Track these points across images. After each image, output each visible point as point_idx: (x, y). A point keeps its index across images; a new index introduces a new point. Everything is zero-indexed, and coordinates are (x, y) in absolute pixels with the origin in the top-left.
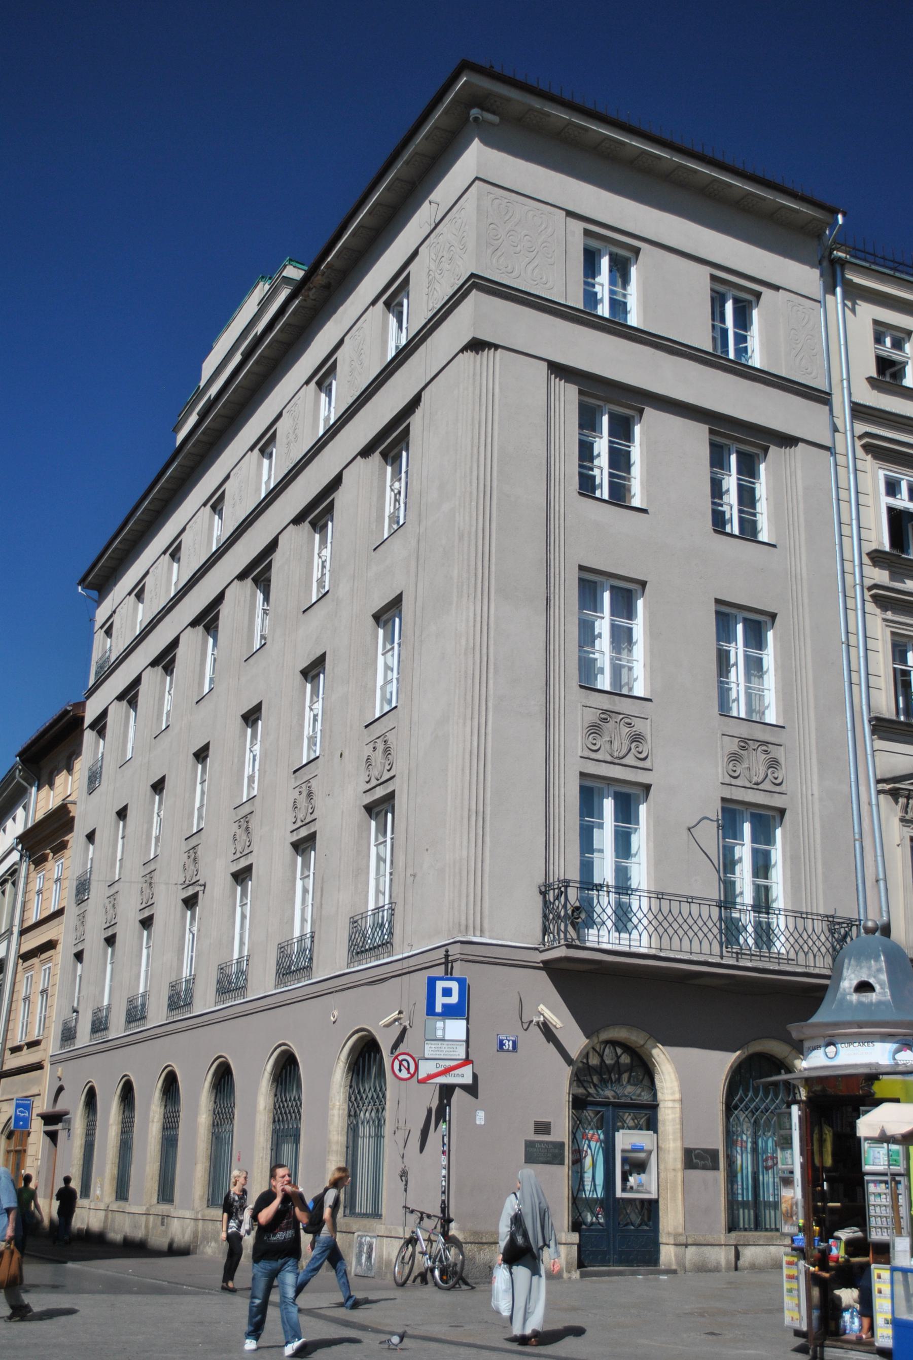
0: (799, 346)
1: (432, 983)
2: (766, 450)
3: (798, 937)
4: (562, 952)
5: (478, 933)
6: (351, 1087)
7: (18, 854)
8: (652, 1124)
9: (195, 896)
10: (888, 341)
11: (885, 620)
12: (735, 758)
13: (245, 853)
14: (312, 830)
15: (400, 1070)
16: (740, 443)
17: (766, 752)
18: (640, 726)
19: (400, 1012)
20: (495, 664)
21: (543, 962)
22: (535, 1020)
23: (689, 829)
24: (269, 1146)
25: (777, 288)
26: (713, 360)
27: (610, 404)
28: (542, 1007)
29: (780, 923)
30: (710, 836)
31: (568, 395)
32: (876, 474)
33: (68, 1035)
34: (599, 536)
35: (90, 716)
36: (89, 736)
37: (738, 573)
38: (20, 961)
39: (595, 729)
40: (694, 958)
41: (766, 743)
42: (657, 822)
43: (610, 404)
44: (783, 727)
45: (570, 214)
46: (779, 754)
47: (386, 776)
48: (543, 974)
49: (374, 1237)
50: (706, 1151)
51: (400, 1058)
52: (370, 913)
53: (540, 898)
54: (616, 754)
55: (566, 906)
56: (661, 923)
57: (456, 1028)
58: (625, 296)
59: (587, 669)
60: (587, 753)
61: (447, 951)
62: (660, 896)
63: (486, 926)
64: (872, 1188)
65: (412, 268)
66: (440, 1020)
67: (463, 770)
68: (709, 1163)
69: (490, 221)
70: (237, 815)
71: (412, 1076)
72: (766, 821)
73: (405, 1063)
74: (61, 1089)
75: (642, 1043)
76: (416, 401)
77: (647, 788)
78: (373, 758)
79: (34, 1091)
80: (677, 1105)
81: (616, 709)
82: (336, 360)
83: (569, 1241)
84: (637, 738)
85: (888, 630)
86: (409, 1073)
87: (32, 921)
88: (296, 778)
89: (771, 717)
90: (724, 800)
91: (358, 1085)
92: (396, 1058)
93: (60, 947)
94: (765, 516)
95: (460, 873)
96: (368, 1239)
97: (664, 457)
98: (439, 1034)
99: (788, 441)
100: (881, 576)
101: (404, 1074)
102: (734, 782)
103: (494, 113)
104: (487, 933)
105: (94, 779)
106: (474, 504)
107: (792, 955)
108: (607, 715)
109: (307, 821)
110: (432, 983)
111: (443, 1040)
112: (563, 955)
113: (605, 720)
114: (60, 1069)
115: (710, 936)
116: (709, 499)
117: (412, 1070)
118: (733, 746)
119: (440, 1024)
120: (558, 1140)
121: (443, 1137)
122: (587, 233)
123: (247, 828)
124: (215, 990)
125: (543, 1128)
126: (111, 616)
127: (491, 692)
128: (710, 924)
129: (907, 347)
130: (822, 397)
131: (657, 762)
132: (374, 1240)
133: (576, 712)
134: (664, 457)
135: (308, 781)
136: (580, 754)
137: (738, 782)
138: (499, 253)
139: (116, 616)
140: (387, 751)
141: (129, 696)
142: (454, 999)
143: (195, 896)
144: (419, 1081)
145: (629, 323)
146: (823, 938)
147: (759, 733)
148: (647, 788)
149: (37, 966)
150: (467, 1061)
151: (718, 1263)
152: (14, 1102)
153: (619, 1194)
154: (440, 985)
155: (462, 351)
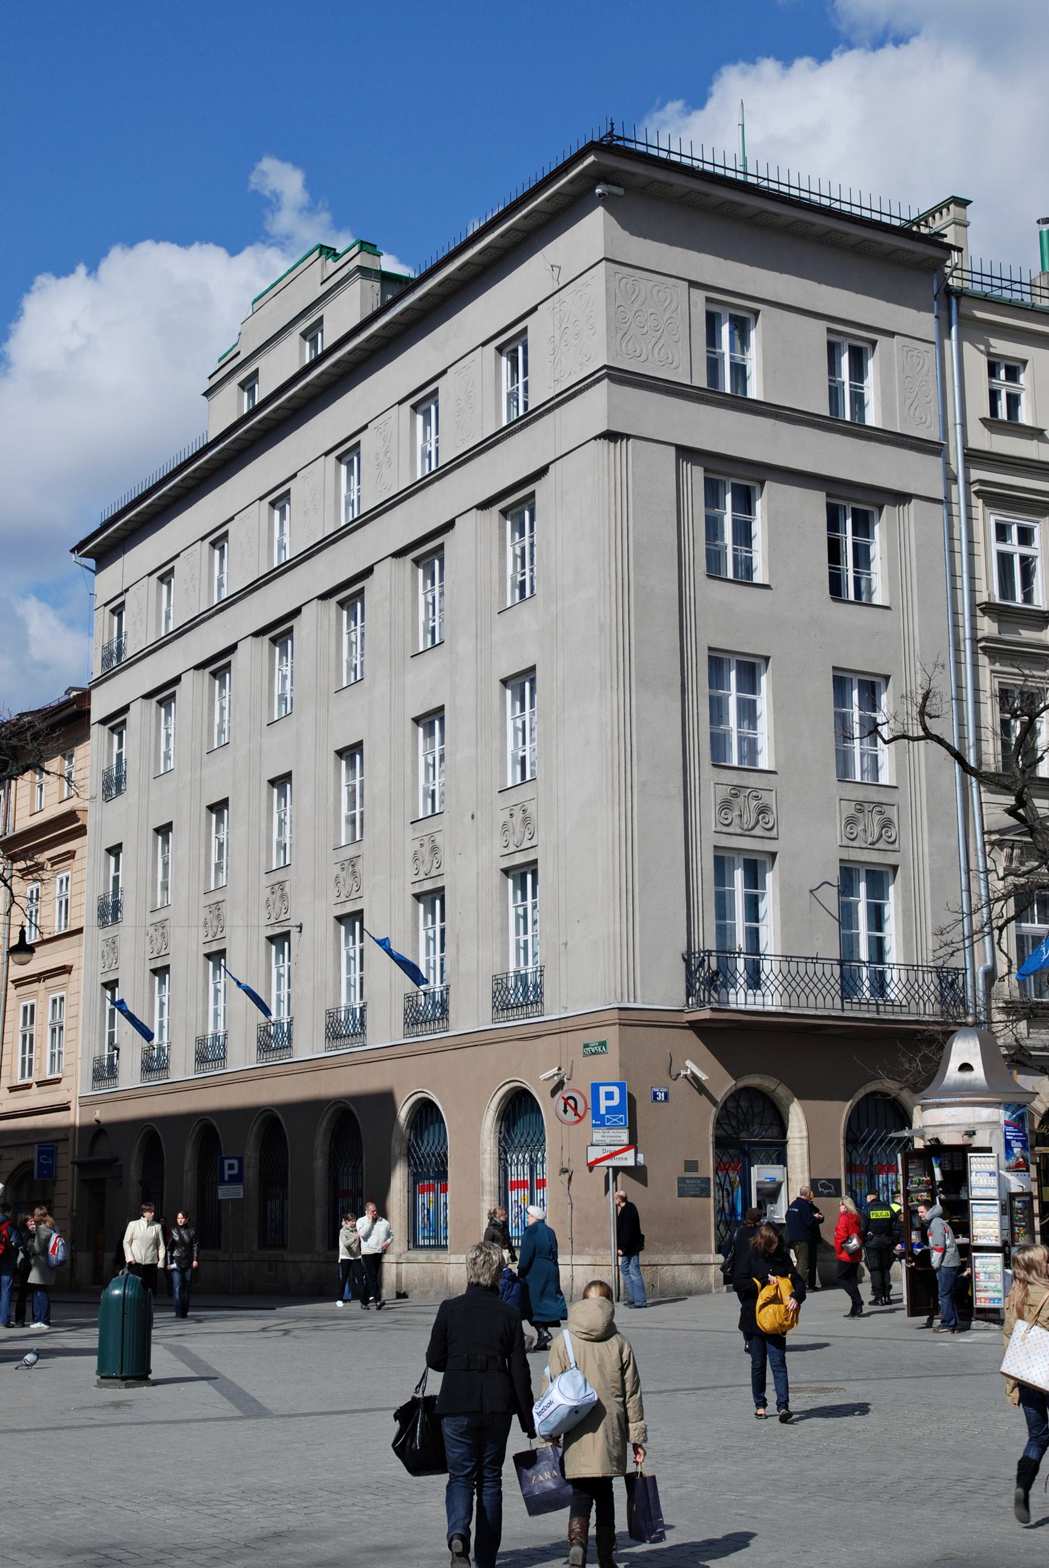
0: (914, 394)
2: (880, 509)
3: (909, 985)
4: (706, 1014)
5: (632, 999)
6: (500, 1132)
8: (781, 1159)
10: (1003, 373)
11: (992, 671)
12: (851, 821)
13: (351, 897)
14: (440, 885)
16: (852, 507)
17: (881, 813)
18: (769, 799)
19: (560, 1069)
20: (638, 752)
21: (687, 1022)
22: (683, 1073)
23: (811, 891)
24: (406, 1189)
25: (892, 334)
26: (830, 424)
27: (735, 480)
28: (688, 1063)
29: (893, 976)
30: (831, 897)
31: (695, 476)
32: (987, 520)
34: (727, 616)
35: (97, 712)
36: (98, 733)
37: (851, 637)
39: (726, 805)
40: (819, 1013)
42: (784, 887)
44: (896, 787)
45: (693, 284)
46: (892, 813)
47: (434, 873)
48: (690, 1033)
53: (683, 965)
54: (745, 827)
55: (706, 974)
56: (789, 982)
58: (743, 360)
59: (718, 744)
62: (788, 958)
64: (975, 1208)
67: (613, 852)
68: (832, 1191)
69: (617, 304)
72: (879, 880)
75: (773, 1088)
77: (773, 855)
78: (510, 824)
80: (805, 1142)
84: (763, 810)
85: (997, 680)
88: (414, 829)
89: (884, 779)
90: (841, 860)
94: (879, 576)
95: (615, 946)
97: (784, 529)
99: (902, 498)
100: (988, 627)
102: (851, 843)
103: (618, 185)
104: (639, 999)
105: (114, 784)
106: (613, 597)
107: (904, 1003)
113: (736, 796)
114: (98, 1112)
115: (833, 992)
116: (827, 565)
118: (850, 809)
122: (708, 300)
123: (354, 872)
125: (691, 1166)
127: (635, 779)
128: (832, 981)
129: (1022, 378)
131: (783, 829)
133: (711, 787)
134: (784, 529)
136: (714, 829)
137: (855, 844)
138: (628, 337)
140: (526, 821)
141: (163, 695)
145: (749, 396)
146: (932, 988)
147: (874, 795)
148: (773, 855)
149: (41, 994)
155: (595, 438)
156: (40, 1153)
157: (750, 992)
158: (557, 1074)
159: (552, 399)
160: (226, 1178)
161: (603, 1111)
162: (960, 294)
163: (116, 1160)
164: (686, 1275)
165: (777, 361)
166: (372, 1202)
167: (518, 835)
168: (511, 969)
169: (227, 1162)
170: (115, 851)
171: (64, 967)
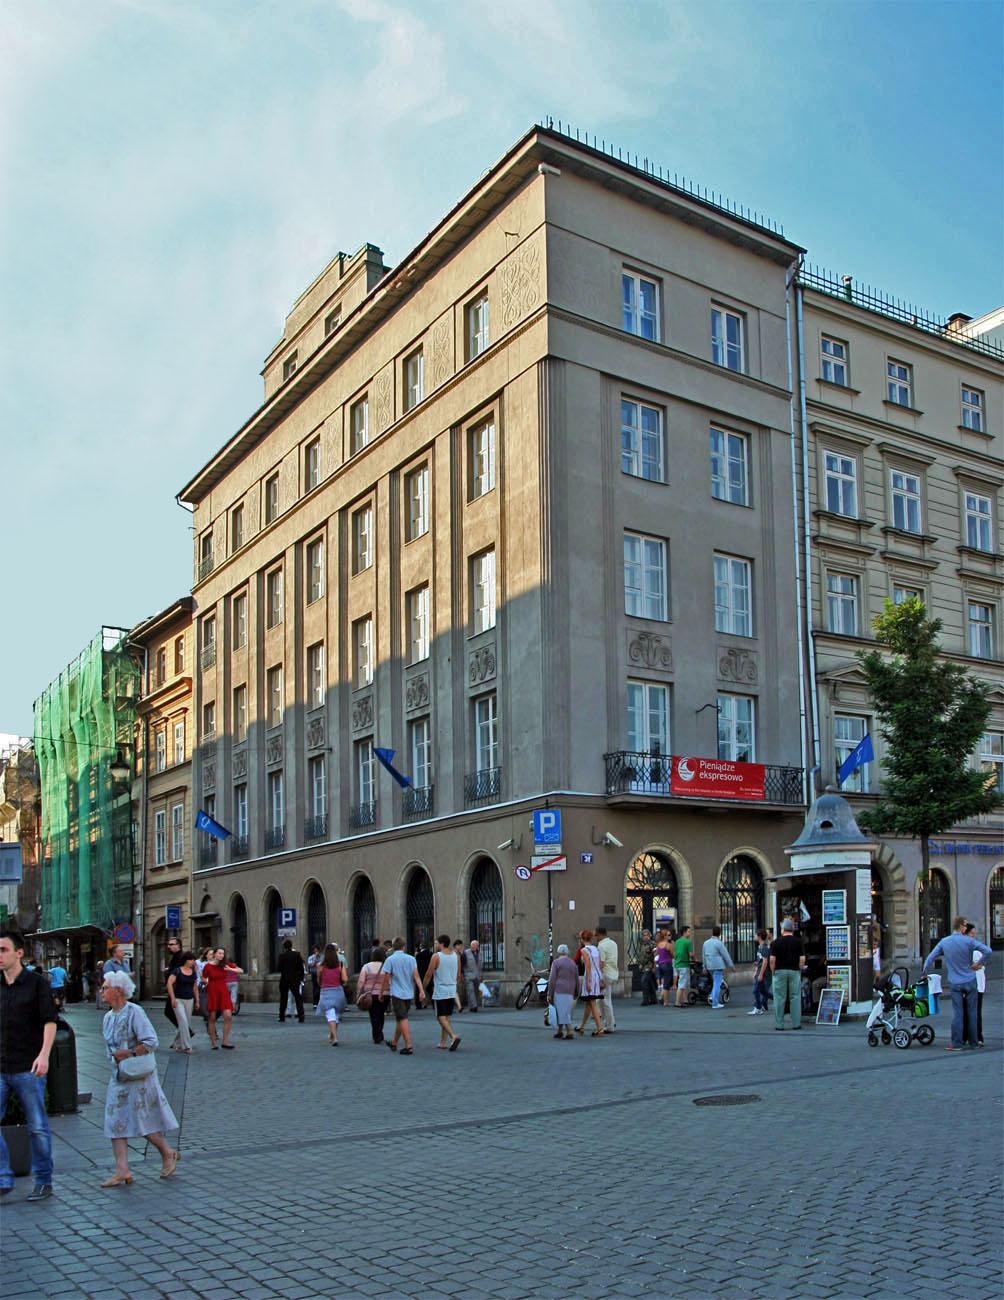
14: (426, 712)
19: (512, 841)
41: (746, 651)
46: (753, 657)
47: (422, 704)
74: (207, 898)
79: (181, 899)
93: (190, 793)
108: (644, 636)
140: (486, 661)
156: (169, 911)
157: (654, 784)
160: (284, 923)
161: (543, 831)
162: (804, 287)
163: (217, 915)
168: (362, 802)
169: (284, 913)
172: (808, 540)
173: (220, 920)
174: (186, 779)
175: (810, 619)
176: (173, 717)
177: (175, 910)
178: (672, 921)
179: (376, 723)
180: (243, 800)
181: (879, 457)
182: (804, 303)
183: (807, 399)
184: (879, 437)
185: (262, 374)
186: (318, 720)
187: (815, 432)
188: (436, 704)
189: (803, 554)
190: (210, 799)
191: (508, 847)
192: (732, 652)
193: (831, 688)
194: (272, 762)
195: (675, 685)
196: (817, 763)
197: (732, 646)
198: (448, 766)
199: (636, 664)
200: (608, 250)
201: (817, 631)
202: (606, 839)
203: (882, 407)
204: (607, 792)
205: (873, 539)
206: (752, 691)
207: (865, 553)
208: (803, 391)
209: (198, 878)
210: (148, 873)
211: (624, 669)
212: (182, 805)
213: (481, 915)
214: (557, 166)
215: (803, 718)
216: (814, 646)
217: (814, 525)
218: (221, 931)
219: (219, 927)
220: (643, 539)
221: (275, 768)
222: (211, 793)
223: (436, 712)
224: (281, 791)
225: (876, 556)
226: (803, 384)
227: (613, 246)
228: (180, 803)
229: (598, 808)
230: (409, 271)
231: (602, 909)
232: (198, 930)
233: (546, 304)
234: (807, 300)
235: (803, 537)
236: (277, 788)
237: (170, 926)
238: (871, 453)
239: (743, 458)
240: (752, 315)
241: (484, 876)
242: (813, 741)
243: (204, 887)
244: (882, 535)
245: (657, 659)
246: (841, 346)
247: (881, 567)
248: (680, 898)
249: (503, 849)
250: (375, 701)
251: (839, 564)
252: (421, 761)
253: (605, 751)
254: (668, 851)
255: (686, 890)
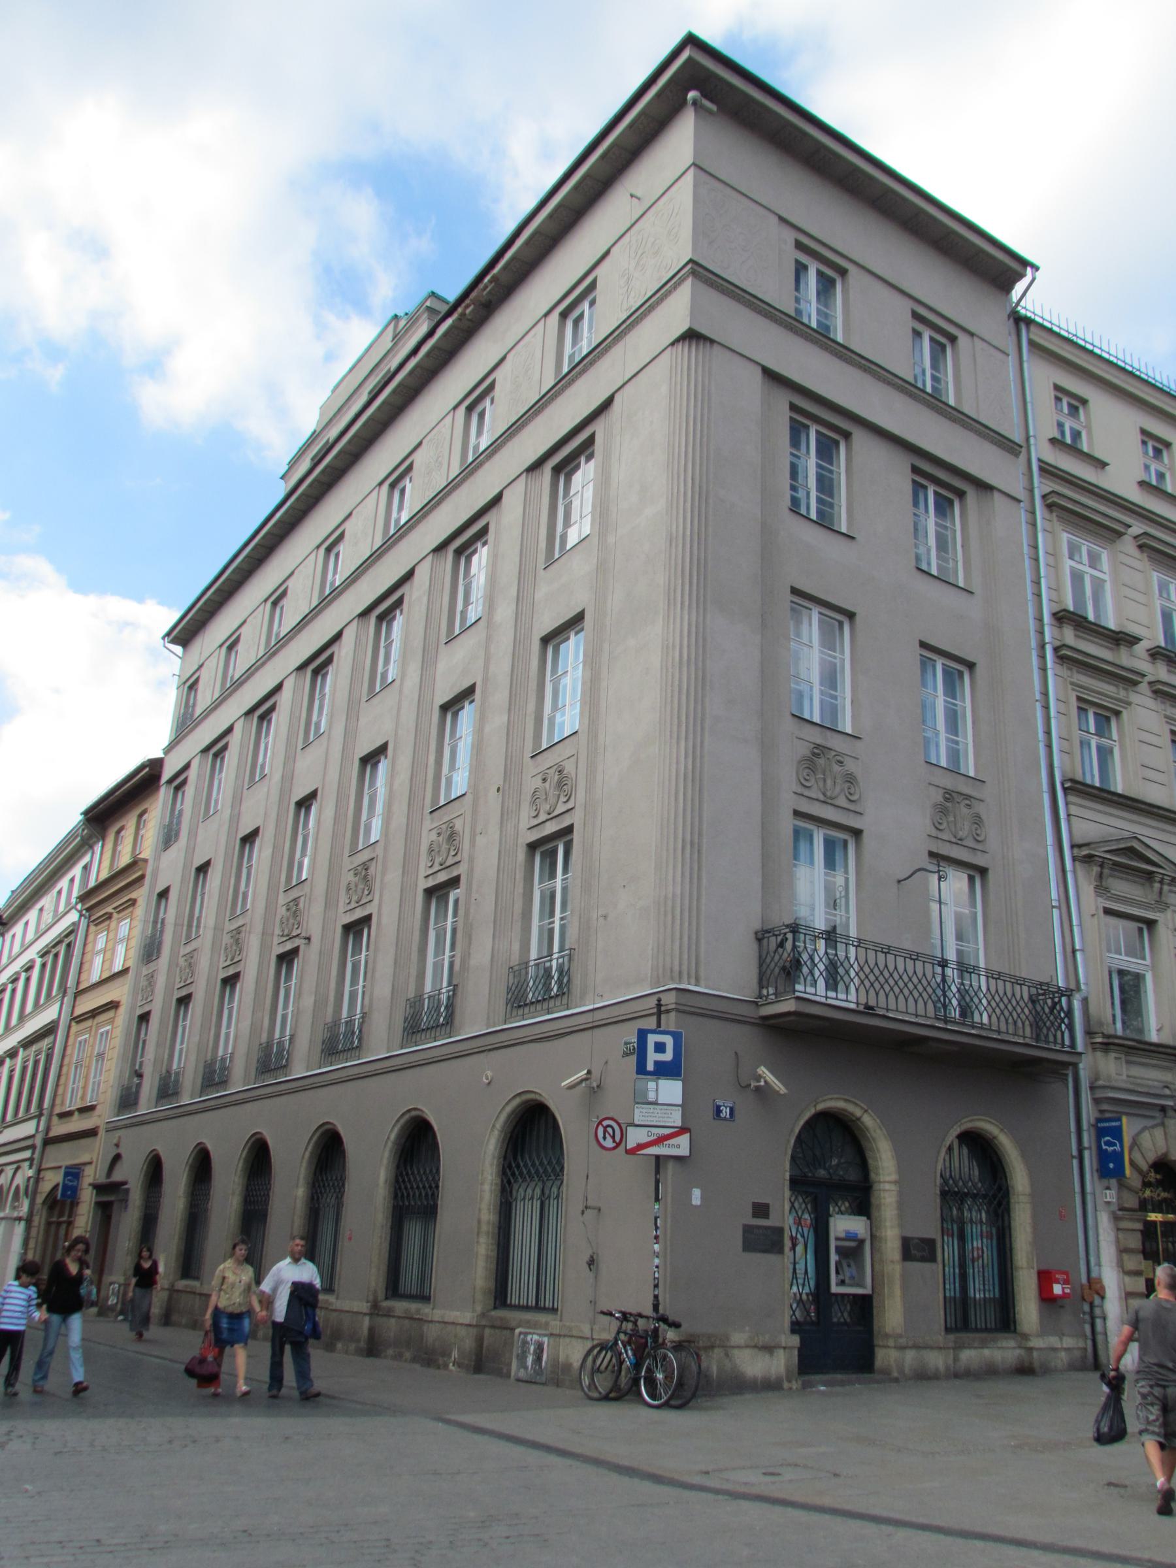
1: (642, 1035)
5: (693, 981)
7: (77, 915)
9: (295, 952)
14: (455, 874)
15: (605, 1138)
19: (589, 1072)
22: (753, 1084)
25: (972, 334)
27: (821, 424)
33: (128, 1100)
38: (73, 1024)
41: (968, 797)
43: (821, 424)
46: (980, 808)
47: (450, 861)
49: (545, 1335)
50: (923, 1240)
51: (605, 1123)
52: (532, 963)
57: (670, 1090)
60: (800, 790)
61: (659, 1000)
63: (702, 974)
65: (599, 272)
66: (652, 1080)
70: (352, 863)
71: (618, 1145)
73: (609, 1130)
74: (117, 1158)
76: (607, 404)
79: (85, 1158)
81: (829, 745)
82: (494, 381)
83: (790, 1344)
84: (850, 779)
86: (614, 1141)
87: (95, 977)
88: (432, 820)
91: (515, 1158)
92: (600, 1123)
93: (122, 1010)
96: (536, 1337)
98: (651, 1096)
101: (609, 1143)
104: (702, 983)
108: (819, 751)
109: (447, 864)
110: (642, 1035)
111: (655, 1103)
112: (793, 1009)
117: (617, 1139)
119: (652, 1085)
120: (778, 1224)
121: (656, 1219)
124: (319, 1050)
125: (761, 1210)
126: (239, 627)
130: (1011, 447)
132: (546, 1340)
134: (872, 482)
135: (450, 821)
139: (204, 669)
140: (560, 784)
142: (668, 1056)
143: (295, 952)
144: (628, 1152)
150: (682, 1130)
151: (937, 1369)
152: (62, 1171)
153: (834, 1289)
154: (652, 1039)
158: (586, 1079)
159: (624, 322)
164: (754, 1366)
165: (869, 318)
166: (696, 1207)
167: (552, 800)
170: (164, 894)
171: (111, 1002)
172: (1049, 650)
173: (127, 1191)
174: (119, 992)
175: (1056, 763)
176: (119, 912)
177: (74, 1173)
178: (862, 1242)
179: (376, 902)
180: (184, 1020)
181: (1135, 552)
182: (1032, 343)
183: (1039, 460)
184: (1137, 528)
185: (282, 478)
186: (296, 900)
187: (1050, 507)
188: (471, 859)
189: (1043, 669)
190: (144, 1018)
191: (582, 1081)
192: (950, 796)
193: (1096, 869)
194: (229, 963)
195: (865, 834)
196: (1083, 987)
197: (949, 787)
198: (481, 954)
199: (806, 793)
200: (775, 220)
201: (1072, 780)
202: (758, 1078)
203: (1136, 487)
204: (760, 996)
205: (1136, 659)
206: (979, 860)
207: (1128, 680)
208: (1033, 449)
209: (112, 1128)
210: (55, 1119)
211: (788, 801)
212: (109, 1027)
213: (520, 1205)
214: (712, 101)
215: (1056, 912)
216: (1067, 804)
217: (1056, 631)
218: (126, 1207)
219: (125, 1201)
220: (815, 613)
221: (231, 971)
222: (146, 1009)
223: (471, 870)
224: (236, 1004)
225: (1144, 687)
226: (1032, 441)
227: (784, 215)
228: (108, 1024)
229: (753, 1024)
230: (486, 287)
231: (749, 1210)
232: (98, 1204)
233: (691, 261)
234: (1032, 336)
235: (1042, 646)
236: (231, 1000)
237: (63, 1194)
238: (1127, 545)
239: (842, 652)
240: (963, 340)
241: (531, 1133)
242: (1074, 951)
243: (115, 1141)
244: (1149, 659)
245: (838, 789)
246: (1078, 404)
247: (1150, 702)
248: (873, 1200)
249: (571, 1087)
250: (380, 868)
251: (1094, 691)
252: (439, 949)
253: (757, 925)
254: (858, 1112)
255: (887, 1186)
